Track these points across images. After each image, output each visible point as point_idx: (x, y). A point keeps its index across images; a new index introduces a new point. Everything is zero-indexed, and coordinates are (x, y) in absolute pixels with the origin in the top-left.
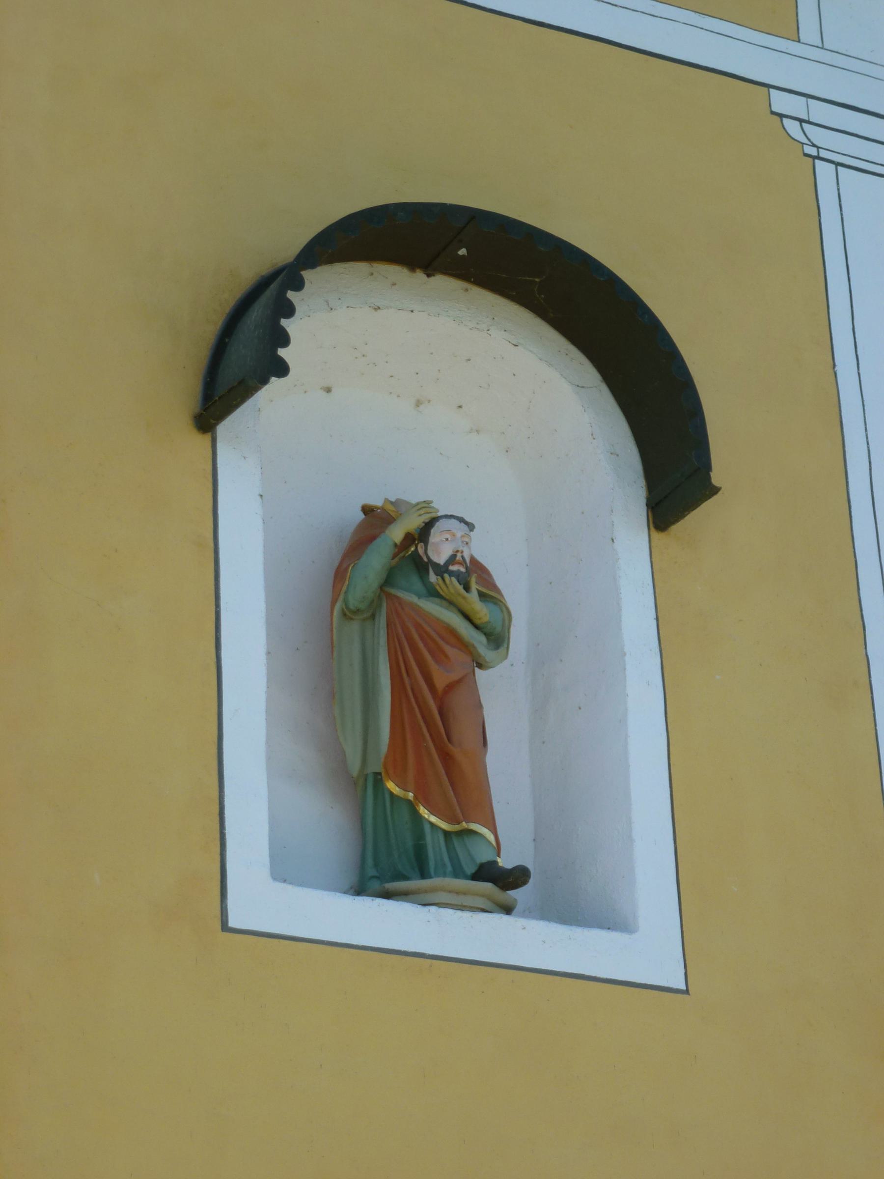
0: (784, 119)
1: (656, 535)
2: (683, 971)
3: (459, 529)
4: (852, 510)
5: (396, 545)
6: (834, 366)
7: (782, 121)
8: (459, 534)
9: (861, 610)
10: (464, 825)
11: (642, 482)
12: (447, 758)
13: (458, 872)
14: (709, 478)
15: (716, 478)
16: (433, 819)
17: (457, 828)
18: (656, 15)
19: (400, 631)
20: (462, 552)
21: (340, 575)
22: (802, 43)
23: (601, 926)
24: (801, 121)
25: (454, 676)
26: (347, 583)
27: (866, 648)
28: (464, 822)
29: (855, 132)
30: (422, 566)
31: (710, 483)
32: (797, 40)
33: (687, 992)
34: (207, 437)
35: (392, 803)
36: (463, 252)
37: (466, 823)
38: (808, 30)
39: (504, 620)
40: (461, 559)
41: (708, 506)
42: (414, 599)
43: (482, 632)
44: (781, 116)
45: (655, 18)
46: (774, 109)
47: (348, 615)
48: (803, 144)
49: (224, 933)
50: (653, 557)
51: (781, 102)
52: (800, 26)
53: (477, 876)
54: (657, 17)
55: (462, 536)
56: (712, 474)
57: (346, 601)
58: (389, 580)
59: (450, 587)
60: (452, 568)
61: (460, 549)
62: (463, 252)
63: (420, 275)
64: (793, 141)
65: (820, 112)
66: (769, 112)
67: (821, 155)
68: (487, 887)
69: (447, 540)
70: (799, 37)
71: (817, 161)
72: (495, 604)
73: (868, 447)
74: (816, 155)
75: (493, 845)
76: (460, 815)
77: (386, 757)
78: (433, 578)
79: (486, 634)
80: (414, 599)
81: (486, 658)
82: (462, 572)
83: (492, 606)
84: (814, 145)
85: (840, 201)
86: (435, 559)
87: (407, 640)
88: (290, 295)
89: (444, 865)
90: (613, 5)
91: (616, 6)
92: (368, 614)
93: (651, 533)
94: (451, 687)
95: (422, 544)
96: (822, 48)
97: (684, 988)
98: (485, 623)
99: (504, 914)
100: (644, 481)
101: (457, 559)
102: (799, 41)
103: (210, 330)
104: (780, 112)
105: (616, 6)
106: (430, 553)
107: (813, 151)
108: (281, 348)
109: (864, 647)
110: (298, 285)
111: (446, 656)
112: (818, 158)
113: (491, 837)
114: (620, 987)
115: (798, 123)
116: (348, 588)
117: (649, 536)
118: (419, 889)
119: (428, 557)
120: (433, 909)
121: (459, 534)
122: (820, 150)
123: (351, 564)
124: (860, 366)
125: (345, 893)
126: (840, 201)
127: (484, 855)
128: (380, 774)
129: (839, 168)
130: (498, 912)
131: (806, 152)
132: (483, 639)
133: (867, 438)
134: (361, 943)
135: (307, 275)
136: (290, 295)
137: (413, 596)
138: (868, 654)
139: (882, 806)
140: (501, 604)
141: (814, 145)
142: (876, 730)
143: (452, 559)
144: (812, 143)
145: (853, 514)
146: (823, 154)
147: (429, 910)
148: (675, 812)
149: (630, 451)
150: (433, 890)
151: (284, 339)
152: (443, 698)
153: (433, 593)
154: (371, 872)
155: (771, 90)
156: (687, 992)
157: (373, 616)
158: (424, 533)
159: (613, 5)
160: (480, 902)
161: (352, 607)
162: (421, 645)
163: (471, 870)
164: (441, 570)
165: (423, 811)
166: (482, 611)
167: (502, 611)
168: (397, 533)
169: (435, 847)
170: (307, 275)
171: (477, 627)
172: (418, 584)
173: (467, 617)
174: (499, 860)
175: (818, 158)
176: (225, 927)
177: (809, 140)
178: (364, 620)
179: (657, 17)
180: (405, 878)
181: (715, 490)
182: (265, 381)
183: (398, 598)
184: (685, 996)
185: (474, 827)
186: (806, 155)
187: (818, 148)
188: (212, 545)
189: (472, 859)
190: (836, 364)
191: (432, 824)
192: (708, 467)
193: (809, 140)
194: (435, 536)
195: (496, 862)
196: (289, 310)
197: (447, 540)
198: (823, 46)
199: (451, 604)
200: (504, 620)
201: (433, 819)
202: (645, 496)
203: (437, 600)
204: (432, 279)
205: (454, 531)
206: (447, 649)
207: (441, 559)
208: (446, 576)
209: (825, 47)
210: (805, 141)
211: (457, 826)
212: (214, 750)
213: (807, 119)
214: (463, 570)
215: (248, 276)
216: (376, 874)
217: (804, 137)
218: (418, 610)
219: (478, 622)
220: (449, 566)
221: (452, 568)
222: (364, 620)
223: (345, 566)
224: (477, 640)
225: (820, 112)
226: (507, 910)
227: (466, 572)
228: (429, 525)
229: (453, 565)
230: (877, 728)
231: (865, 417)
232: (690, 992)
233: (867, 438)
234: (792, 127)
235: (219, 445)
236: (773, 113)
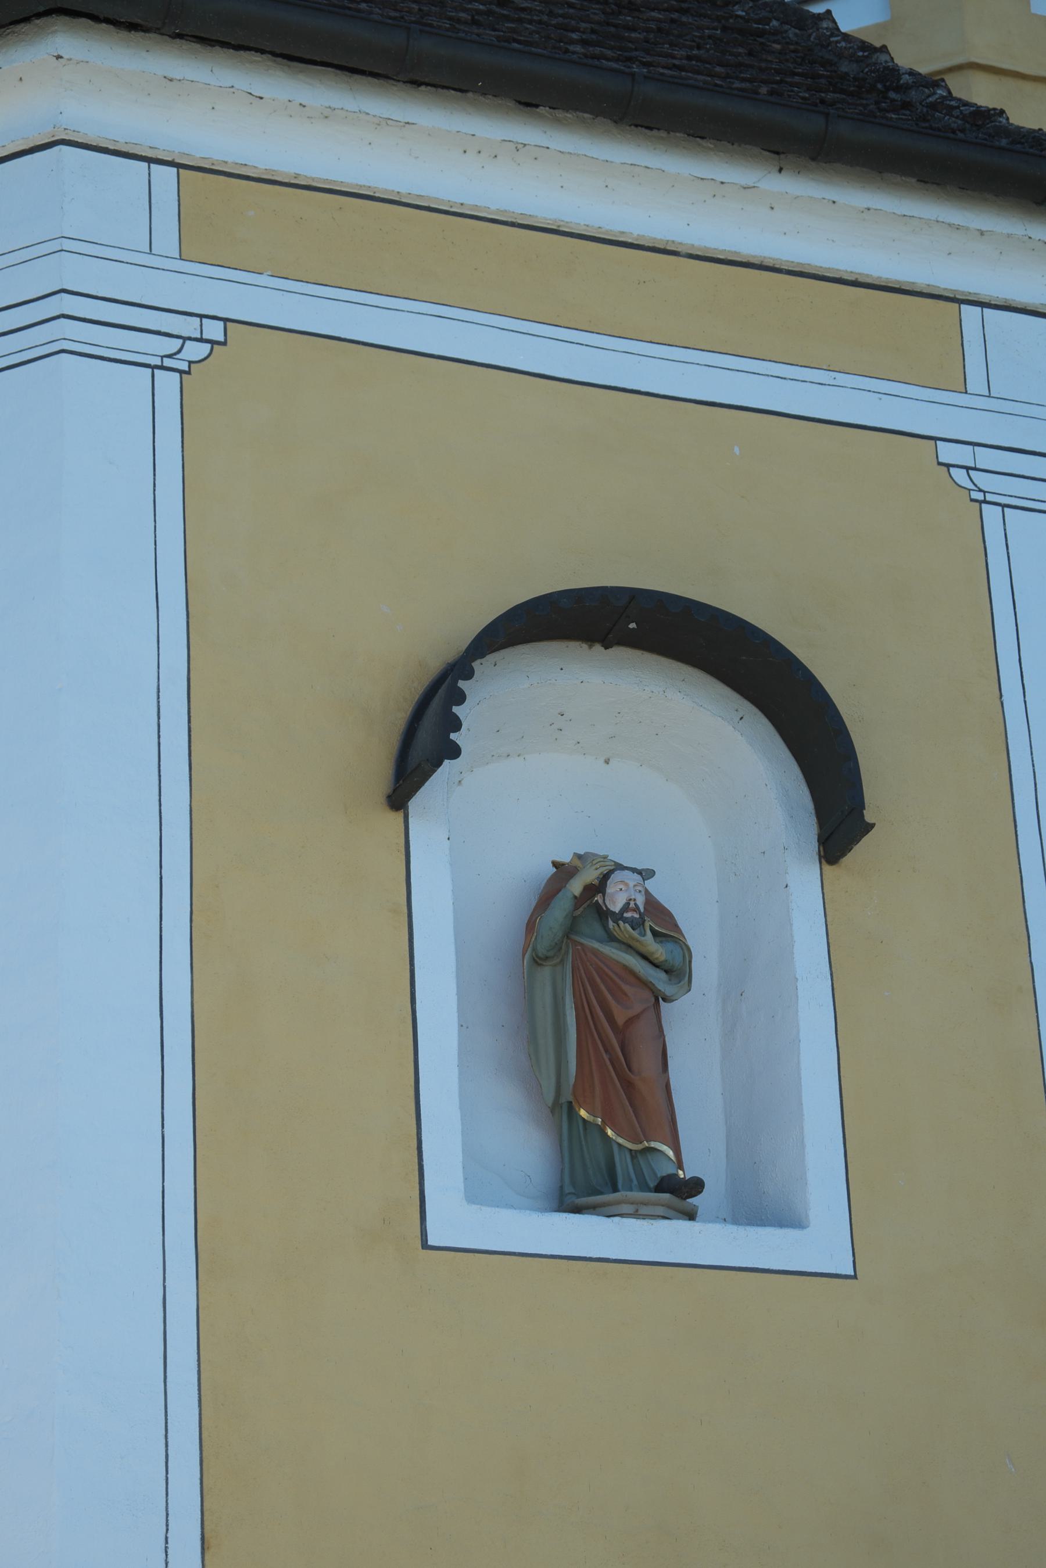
0: (952, 470)
1: (827, 868)
2: (852, 1259)
3: (633, 879)
4: (1018, 829)
5: (575, 897)
6: (1001, 696)
7: (949, 470)
8: (631, 884)
9: (1026, 921)
10: (646, 1144)
11: (814, 820)
12: (628, 1086)
13: (644, 1187)
14: (863, 815)
15: (869, 816)
16: (621, 1141)
17: (639, 1147)
18: (824, 383)
19: (583, 975)
20: (635, 900)
21: (531, 926)
22: (970, 394)
23: (781, 1224)
24: (968, 469)
25: (631, 1013)
26: (535, 934)
27: (1030, 956)
28: (645, 1142)
29: (1021, 473)
30: (603, 914)
31: (864, 820)
32: (964, 391)
33: (855, 1277)
34: (400, 815)
35: (585, 1129)
36: (632, 626)
37: (647, 1142)
38: (976, 381)
39: (684, 956)
40: (634, 906)
41: (867, 842)
42: (596, 945)
43: (662, 969)
44: (948, 466)
45: (823, 386)
46: (940, 460)
47: (538, 961)
48: (970, 490)
49: (424, 1251)
50: (824, 888)
51: (948, 453)
52: (967, 377)
53: (659, 1189)
54: (825, 385)
55: (635, 886)
56: (865, 812)
57: (534, 950)
58: (572, 928)
59: (625, 933)
60: (625, 915)
61: (633, 897)
62: (632, 626)
63: (598, 648)
64: (960, 488)
65: (986, 458)
66: (936, 463)
67: (988, 499)
68: (666, 1196)
69: (621, 890)
70: (966, 388)
71: (984, 506)
72: (676, 942)
73: (1034, 770)
74: (983, 499)
75: (672, 1160)
76: (642, 1136)
77: (575, 1085)
78: (611, 924)
79: (666, 972)
80: (596, 945)
81: (666, 993)
82: (636, 918)
83: (670, 946)
84: (980, 490)
85: (1006, 540)
86: (612, 908)
87: (591, 985)
88: (461, 684)
89: (631, 1181)
90: (782, 378)
91: (785, 379)
92: (558, 960)
93: (823, 867)
94: (631, 1021)
95: (601, 894)
96: (989, 396)
97: (853, 1274)
98: (662, 962)
99: (685, 1220)
100: (815, 818)
101: (631, 906)
102: (966, 392)
103: (401, 718)
104: (947, 462)
105: (785, 379)
106: (607, 903)
107: (980, 496)
108: (453, 732)
109: (1028, 955)
110: (469, 675)
111: (626, 994)
112: (985, 502)
113: (671, 1153)
114: (792, 1276)
115: (964, 471)
116: (536, 939)
117: (821, 869)
118: (604, 1203)
119: (606, 906)
120: (617, 1219)
121: (631, 884)
122: (986, 494)
123: (538, 916)
124: (1026, 694)
125: (555, 1211)
126: (1006, 540)
127: (666, 1169)
128: (571, 1102)
129: (1006, 509)
130: (678, 1219)
131: (972, 497)
132: (663, 975)
133: (1033, 761)
134: (549, 1253)
135: (476, 665)
136: (461, 684)
137: (594, 941)
138: (1033, 961)
139: (1044, 1099)
140: (681, 942)
141: (980, 490)
142: (1039, 1030)
143: (626, 908)
144: (979, 488)
145: (1018, 833)
146: (989, 497)
147: (613, 1221)
148: (845, 1118)
149: (801, 792)
150: (618, 1203)
151: (456, 725)
152: (623, 1032)
153: (612, 938)
154: (568, 1189)
155: (938, 442)
156: (855, 1277)
157: (562, 962)
158: (599, 887)
159: (782, 378)
160: (660, 1210)
161: (540, 955)
162: (603, 988)
163: (652, 1184)
164: (618, 917)
165: (609, 1132)
166: (659, 951)
167: (682, 949)
168: (576, 887)
169: (623, 1165)
170: (476, 665)
171: (656, 966)
172: (600, 931)
173: (645, 957)
174: (681, 1172)
175: (985, 502)
176: (425, 1245)
177: (975, 485)
178: (555, 965)
179: (825, 385)
180: (601, 1193)
181: (869, 827)
182: (439, 764)
183: (582, 944)
184: (855, 1281)
185: (653, 1144)
186: (972, 500)
187: (985, 492)
188: (406, 911)
189: (655, 1174)
190: (1003, 694)
191: (619, 1145)
192: (862, 806)
193: (975, 485)
194: (611, 888)
195: (677, 1175)
196: (460, 698)
197: (621, 890)
198: (990, 394)
199: (629, 947)
200: (684, 956)
201: (621, 1141)
202: (817, 833)
203: (615, 944)
204: (610, 651)
205: (626, 881)
206: (626, 988)
207: (616, 907)
208: (621, 923)
209: (992, 395)
210: (971, 486)
211: (639, 1145)
212: (412, 1093)
213: (974, 466)
214: (637, 916)
215: (435, 665)
216: (573, 1191)
217: (972, 484)
218: (596, 953)
219: (656, 961)
220: (623, 914)
221: (625, 915)
222: (555, 965)
223: (534, 919)
224: (658, 979)
225: (986, 458)
226: (691, 1215)
227: (640, 918)
228: (605, 878)
229: (627, 912)
230: (1040, 1028)
231: (1030, 741)
232: (858, 1276)
233: (1033, 761)
234: (959, 475)
235: (411, 820)
236: (940, 464)
